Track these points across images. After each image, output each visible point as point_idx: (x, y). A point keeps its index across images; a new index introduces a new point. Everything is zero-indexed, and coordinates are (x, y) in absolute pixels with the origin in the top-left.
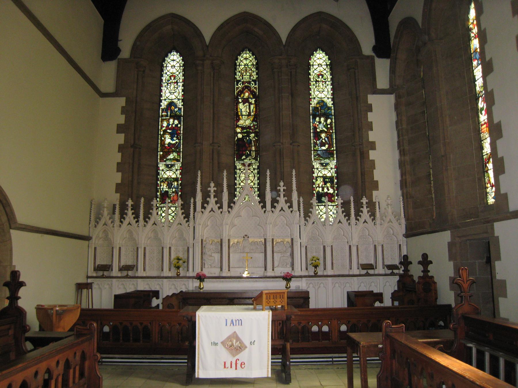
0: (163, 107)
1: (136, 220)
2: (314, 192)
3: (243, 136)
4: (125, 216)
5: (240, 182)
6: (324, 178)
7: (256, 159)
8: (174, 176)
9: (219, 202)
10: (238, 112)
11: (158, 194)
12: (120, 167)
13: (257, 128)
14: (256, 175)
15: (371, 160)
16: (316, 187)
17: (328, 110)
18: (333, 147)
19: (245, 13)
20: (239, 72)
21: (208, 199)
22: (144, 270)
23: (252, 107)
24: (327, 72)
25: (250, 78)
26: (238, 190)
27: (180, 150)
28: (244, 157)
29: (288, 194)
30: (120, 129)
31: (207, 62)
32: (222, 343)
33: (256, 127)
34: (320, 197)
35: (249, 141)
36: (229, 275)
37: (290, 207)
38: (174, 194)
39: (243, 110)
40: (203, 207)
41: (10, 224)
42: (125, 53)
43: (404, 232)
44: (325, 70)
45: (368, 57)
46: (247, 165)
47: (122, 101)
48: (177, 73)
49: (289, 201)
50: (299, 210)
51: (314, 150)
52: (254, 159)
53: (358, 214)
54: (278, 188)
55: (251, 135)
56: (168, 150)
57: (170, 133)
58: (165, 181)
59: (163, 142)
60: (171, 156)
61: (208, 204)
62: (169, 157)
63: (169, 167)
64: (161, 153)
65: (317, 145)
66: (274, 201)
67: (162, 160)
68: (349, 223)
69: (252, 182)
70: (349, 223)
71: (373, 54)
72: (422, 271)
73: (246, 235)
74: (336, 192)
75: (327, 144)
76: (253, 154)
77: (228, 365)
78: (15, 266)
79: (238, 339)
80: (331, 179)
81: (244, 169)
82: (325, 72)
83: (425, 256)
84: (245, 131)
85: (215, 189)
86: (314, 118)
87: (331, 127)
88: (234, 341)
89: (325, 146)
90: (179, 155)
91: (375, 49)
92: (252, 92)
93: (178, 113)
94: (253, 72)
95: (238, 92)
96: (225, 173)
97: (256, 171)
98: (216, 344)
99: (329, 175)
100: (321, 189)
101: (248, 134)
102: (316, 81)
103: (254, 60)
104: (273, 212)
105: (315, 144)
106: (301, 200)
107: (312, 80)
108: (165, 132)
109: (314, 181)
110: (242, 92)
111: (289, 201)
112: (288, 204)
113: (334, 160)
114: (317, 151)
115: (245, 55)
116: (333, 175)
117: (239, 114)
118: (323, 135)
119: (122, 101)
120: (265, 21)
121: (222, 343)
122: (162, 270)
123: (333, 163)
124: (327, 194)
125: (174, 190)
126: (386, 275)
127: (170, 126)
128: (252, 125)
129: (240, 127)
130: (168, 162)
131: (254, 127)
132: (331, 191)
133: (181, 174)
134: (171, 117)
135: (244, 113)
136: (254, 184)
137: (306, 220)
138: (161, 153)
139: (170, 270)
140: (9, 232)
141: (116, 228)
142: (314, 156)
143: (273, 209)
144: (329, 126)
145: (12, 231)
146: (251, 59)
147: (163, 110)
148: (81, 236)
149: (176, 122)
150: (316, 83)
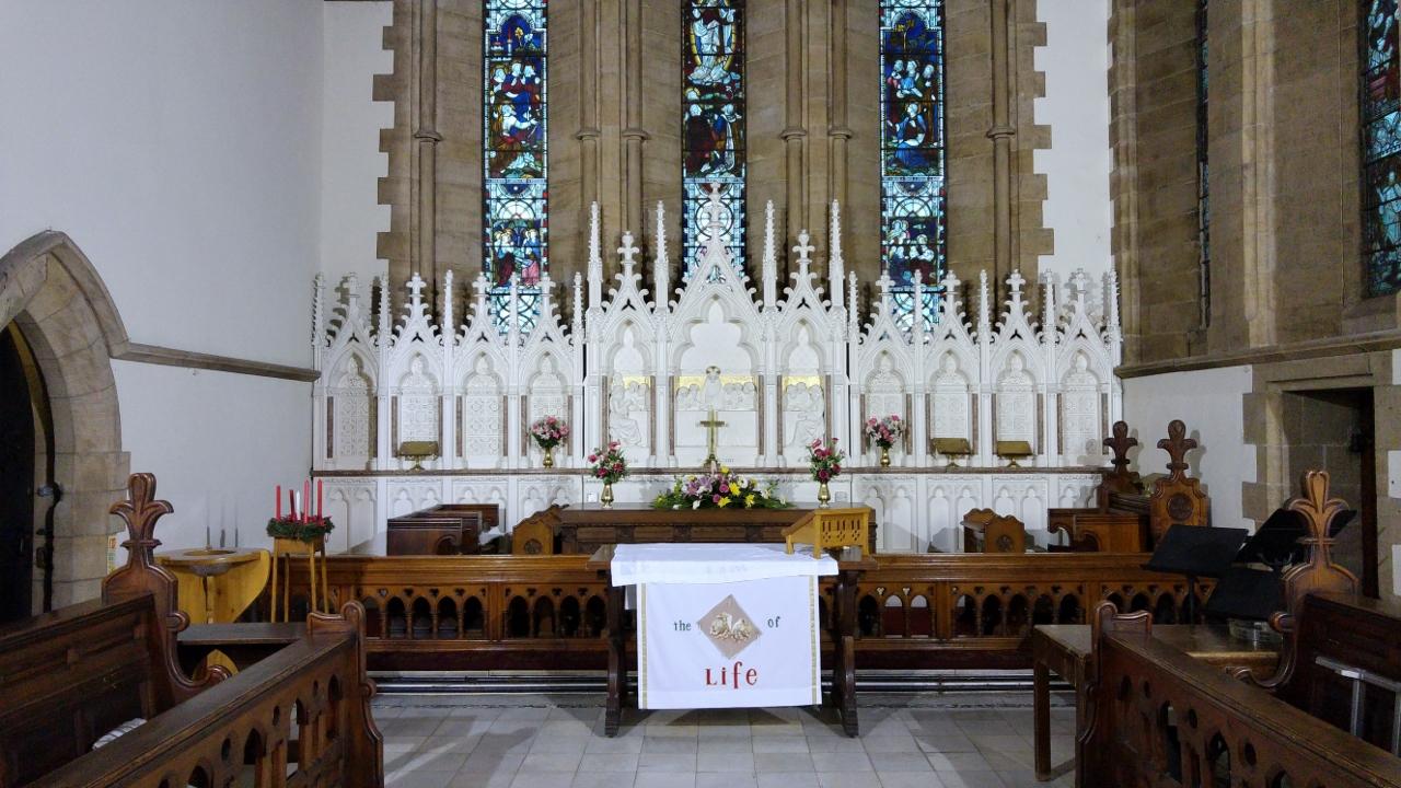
0: (493, 30)
1: (564, 327)
2: (885, 258)
3: (704, 112)
4: (404, 317)
5: (697, 231)
6: (912, 220)
7: (736, 171)
8: (528, 215)
9: (647, 284)
10: (691, 45)
11: (488, 260)
12: (386, 189)
13: (740, 90)
14: (737, 214)
15: (1038, 175)
16: (891, 246)
17: (928, 39)
18: (937, 140)
22: (330, 454)
23: (728, 30)
26: (691, 252)
27: (542, 146)
28: (706, 167)
29: (821, 259)
30: (385, 88)
32: (700, 623)
33: (737, 85)
34: (900, 269)
35: (719, 124)
36: (458, 466)
37: (648, 299)
38: (529, 262)
39: (703, 40)
40: (606, 297)
43: (1117, 362)
46: (715, 190)
50: (846, 305)
51: (887, 149)
52: (731, 172)
54: (795, 249)
56: (509, 146)
57: (513, 102)
58: (506, 227)
59: (496, 124)
60: (519, 163)
62: (513, 165)
63: (516, 192)
64: (493, 154)
65: (896, 134)
66: (784, 282)
67: (494, 172)
68: (975, 339)
69: (727, 232)
70: (975, 339)
72: (1168, 466)
73: (713, 368)
76: (731, 159)
77: (716, 676)
79: (738, 613)
80: (930, 223)
81: (709, 200)
83: (1176, 428)
84: (709, 96)
86: (890, 65)
87: (934, 90)
88: (724, 625)
89: (915, 138)
90: (539, 160)
93: (533, 47)
96: (661, 212)
97: (737, 204)
98: (684, 626)
99: (924, 213)
100: (901, 249)
101: (718, 104)
105: (891, 132)
106: (853, 279)
109: (884, 228)
112: (820, 290)
113: (938, 174)
114: (896, 149)
116: (936, 212)
117: (695, 50)
118: (912, 109)
121: (700, 623)
122: (506, 454)
123: (935, 185)
124: (915, 264)
125: (529, 251)
126: (999, 471)
127: (514, 83)
128: (726, 81)
129: (699, 87)
130: (512, 179)
131: (733, 88)
132: (928, 255)
133: (546, 209)
134: (516, 56)
135: (707, 49)
136: (733, 238)
137: (864, 330)
138: (493, 154)
139: (524, 452)
140: (108, 366)
142: (888, 164)
144: (928, 84)
145: (114, 363)
147: (493, 38)
149: (530, 71)
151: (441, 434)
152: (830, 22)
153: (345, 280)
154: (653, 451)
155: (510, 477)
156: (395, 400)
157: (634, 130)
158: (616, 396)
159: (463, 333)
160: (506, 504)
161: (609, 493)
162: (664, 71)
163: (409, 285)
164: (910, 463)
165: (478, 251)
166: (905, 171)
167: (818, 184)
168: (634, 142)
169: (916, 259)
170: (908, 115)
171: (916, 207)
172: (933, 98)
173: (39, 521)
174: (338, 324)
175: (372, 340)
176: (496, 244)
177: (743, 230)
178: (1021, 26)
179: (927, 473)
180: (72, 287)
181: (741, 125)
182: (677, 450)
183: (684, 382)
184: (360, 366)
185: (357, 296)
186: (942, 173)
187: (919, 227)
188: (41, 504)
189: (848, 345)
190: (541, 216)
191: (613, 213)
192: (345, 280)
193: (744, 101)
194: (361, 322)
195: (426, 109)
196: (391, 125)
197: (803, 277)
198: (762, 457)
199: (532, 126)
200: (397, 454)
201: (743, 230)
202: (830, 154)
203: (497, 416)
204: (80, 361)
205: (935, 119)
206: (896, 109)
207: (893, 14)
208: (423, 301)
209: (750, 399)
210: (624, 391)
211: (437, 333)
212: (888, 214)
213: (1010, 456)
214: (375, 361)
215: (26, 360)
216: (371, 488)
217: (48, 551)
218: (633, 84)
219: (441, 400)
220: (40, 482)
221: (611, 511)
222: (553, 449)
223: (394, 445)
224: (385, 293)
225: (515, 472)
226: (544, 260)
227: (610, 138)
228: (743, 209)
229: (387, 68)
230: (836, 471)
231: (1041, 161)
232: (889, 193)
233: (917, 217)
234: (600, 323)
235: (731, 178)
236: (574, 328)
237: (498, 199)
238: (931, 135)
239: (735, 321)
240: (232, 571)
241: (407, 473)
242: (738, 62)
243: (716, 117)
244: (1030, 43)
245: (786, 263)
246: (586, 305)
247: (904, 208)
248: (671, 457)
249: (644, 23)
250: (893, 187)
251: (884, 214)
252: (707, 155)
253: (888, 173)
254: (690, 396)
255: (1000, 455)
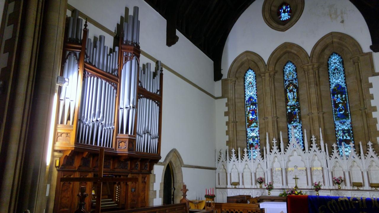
2: (337, 139)
3: (291, 111)
6: (343, 130)
7: (299, 122)
8: (255, 135)
9: (279, 148)
10: (287, 98)
12: (227, 133)
13: (299, 105)
14: (300, 132)
15: (374, 118)
16: (338, 136)
19: (285, 43)
20: (286, 75)
21: (273, 147)
22: (219, 184)
23: (295, 94)
24: (340, 66)
25: (293, 78)
28: (293, 122)
29: (318, 141)
30: (226, 114)
31: (267, 74)
36: (243, 187)
38: (256, 144)
39: (290, 96)
40: (271, 152)
41: (181, 165)
42: (225, 76)
44: (339, 65)
45: (367, 54)
47: (225, 100)
48: (253, 81)
49: (319, 146)
50: (325, 151)
52: (298, 123)
53: (366, 152)
55: (296, 110)
56: (251, 122)
57: (251, 113)
60: (253, 125)
61: (273, 150)
62: (252, 126)
63: (252, 131)
67: (248, 127)
68: (360, 158)
71: (371, 51)
73: (297, 167)
74: (352, 138)
75: (344, 110)
76: (298, 120)
78: (184, 183)
80: (348, 131)
82: (339, 66)
84: (292, 107)
85: (316, 139)
86: (333, 96)
87: (346, 100)
89: (342, 111)
91: (371, 47)
92: (295, 86)
93: (255, 102)
94: (294, 74)
95: (287, 86)
99: (346, 128)
101: (294, 109)
102: (333, 73)
103: (294, 67)
104: (309, 152)
105: (335, 111)
107: (330, 73)
108: (249, 112)
109: (336, 132)
110: (288, 86)
111: (319, 146)
115: (288, 65)
116: (350, 128)
117: (288, 98)
118: (340, 105)
119: (225, 100)
120: (297, 45)
122: (252, 185)
123: (348, 121)
125: (256, 142)
127: (251, 109)
128: (296, 104)
130: (252, 128)
132: (349, 138)
133: (259, 134)
134: (251, 104)
135: (291, 98)
136: (300, 137)
137: (330, 156)
139: (256, 184)
140: (181, 168)
141: (228, 163)
142: (335, 118)
143: (309, 151)
144: (344, 99)
145: (182, 168)
146: (292, 67)
148: (211, 168)
149: (254, 107)
150: (333, 75)
151: (239, 181)
152: (316, 90)
153: (221, 150)
154: (283, 185)
155: (253, 190)
156: (230, 174)
157: (275, 117)
158: (274, 172)
159: (242, 160)
160: (253, 195)
161: (270, 193)
162: (282, 104)
163: (232, 151)
164: (346, 188)
165: (246, 143)
166: (340, 119)
167: (316, 124)
168: (275, 119)
169: (346, 139)
170: (340, 107)
171: (344, 127)
172: (346, 102)
173: (172, 194)
174: (220, 159)
175: (226, 162)
176: (249, 141)
177: (302, 135)
178: (365, 84)
179: (350, 191)
180: (176, 156)
181: (299, 113)
182: (288, 184)
183: (289, 169)
184: (224, 167)
185: (223, 153)
186: (350, 119)
187: (346, 131)
188: (172, 191)
189: (327, 160)
190: (258, 135)
191: (272, 134)
192: (221, 150)
193: (300, 108)
194: (224, 158)
195: (234, 117)
196: (228, 121)
197: (314, 145)
198: (308, 186)
199: (255, 117)
200: (231, 185)
201: (302, 135)
202: (319, 118)
203: (250, 177)
204: (177, 168)
205: (347, 107)
206: (336, 106)
207: (333, 85)
208: (235, 154)
209: (305, 173)
210: (276, 171)
211: (263, 159)
212: (337, 129)
213: (358, 186)
214: (226, 166)
215: (171, 170)
216: (227, 191)
217: (173, 198)
218: (274, 108)
219: (239, 173)
220: (172, 187)
221: (270, 196)
222: (262, 184)
223: (231, 183)
224: (228, 153)
225: (254, 189)
226: (259, 144)
227: (270, 119)
228: (302, 130)
229: (227, 110)
230: (320, 189)
231: (375, 115)
232: (337, 124)
233: (345, 129)
234: (269, 157)
235: (298, 124)
236: (264, 158)
237: (249, 132)
238: (346, 110)
239: (300, 155)
240: (199, 203)
241: (356, 190)
242: (298, 100)
243: (294, 112)
244: (368, 88)
245: (311, 142)
246: (266, 153)
247: (341, 127)
248: (287, 186)
249: (276, 95)
250: (337, 123)
251: (336, 129)
252: (293, 120)
253: (336, 120)
254: (291, 172)
255: (372, 187)
